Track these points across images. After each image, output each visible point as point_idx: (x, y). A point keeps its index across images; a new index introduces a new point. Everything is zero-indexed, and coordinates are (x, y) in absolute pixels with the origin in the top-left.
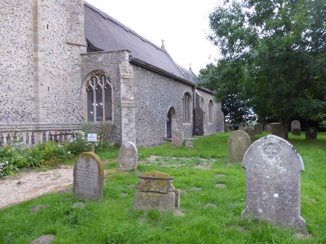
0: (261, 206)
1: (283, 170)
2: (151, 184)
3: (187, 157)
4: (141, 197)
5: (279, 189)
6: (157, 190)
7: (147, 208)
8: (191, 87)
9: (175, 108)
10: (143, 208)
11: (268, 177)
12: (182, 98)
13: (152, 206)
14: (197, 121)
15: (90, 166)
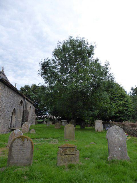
0: (115, 154)
1: (121, 139)
2: (67, 150)
3: (37, 138)
4: (62, 159)
5: (121, 147)
6: (70, 153)
7: (67, 164)
8: (23, 98)
9: (16, 109)
10: (64, 164)
11: (116, 142)
12: (19, 103)
13: (69, 162)
14: (25, 118)
15: (25, 144)
